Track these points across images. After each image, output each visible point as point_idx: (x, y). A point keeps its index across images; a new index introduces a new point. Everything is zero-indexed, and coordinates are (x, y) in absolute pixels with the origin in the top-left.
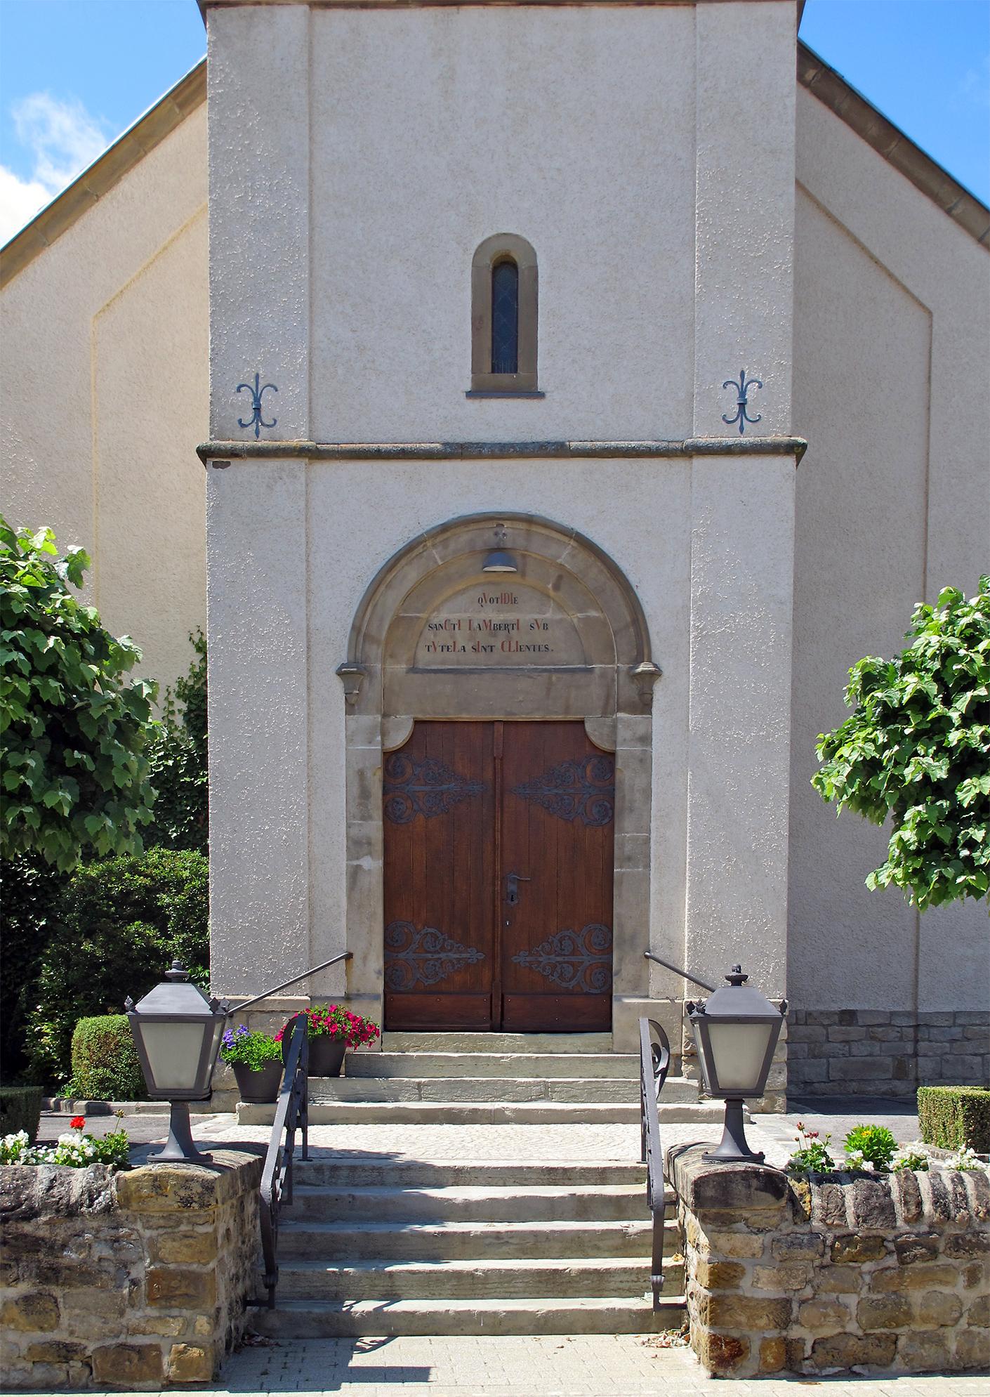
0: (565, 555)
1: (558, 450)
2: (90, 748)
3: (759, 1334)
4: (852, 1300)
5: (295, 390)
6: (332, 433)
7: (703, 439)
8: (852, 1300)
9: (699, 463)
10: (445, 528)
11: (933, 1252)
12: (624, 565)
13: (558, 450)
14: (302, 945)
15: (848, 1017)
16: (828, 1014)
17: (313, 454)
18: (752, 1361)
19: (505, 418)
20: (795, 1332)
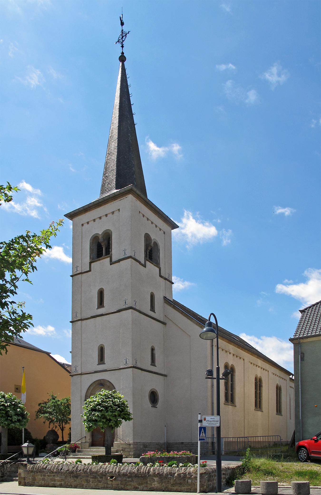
0: (108, 384)
1: (106, 371)
2: (11, 417)
3: (23, 481)
4: (30, 478)
5: (80, 367)
6: (84, 371)
7: (122, 367)
8: (30, 478)
9: (121, 370)
10: (94, 382)
11: (37, 473)
12: (114, 385)
13: (106, 371)
14: (80, 436)
15: (182, 443)
16: (179, 443)
17: (81, 374)
18: (22, 484)
19: (101, 367)
20: (26, 481)
